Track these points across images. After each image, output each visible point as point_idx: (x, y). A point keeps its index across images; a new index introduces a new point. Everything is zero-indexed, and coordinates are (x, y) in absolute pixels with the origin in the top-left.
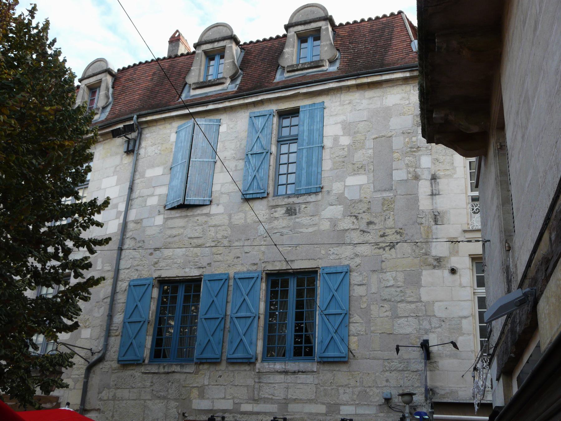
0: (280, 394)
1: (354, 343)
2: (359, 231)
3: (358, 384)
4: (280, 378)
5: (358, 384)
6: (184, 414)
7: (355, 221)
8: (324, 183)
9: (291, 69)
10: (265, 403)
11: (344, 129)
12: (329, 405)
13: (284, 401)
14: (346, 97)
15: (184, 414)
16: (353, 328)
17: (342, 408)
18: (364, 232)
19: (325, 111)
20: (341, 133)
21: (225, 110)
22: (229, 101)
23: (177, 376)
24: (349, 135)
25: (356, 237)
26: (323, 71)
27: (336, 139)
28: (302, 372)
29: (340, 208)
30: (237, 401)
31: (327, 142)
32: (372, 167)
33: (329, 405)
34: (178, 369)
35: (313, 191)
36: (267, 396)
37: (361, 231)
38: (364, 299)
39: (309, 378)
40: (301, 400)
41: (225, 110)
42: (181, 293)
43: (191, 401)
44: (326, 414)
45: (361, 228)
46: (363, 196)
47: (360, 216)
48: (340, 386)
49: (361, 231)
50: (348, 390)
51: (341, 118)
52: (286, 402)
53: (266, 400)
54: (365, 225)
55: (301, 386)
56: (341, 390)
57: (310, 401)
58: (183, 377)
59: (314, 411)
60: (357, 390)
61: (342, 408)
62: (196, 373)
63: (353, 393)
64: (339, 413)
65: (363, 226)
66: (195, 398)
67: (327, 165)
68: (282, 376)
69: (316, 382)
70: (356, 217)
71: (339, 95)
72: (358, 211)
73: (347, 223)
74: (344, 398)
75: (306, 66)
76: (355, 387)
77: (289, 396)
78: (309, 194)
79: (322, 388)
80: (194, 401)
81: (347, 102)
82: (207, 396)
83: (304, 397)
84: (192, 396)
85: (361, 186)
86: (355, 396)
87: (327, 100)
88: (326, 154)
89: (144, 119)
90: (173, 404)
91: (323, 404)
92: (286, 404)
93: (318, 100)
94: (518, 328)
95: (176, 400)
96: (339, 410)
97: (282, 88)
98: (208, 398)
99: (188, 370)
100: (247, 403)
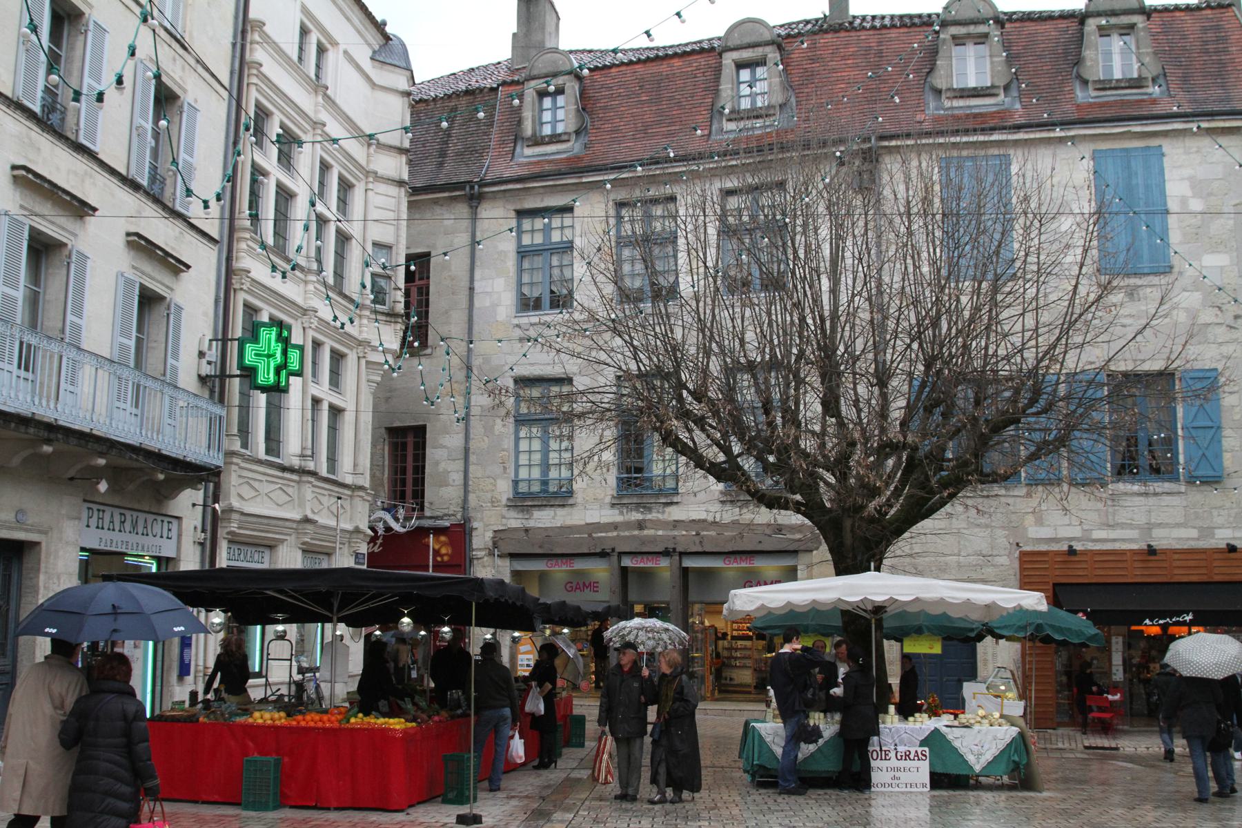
0: (1141, 519)
1: (1228, 460)
2: (1224, 326)
3: (1234, 505)
4: (1137, 500)
5: (1234, 505)
6: (1017, 544)
7: (1219, 313)
8: (1175, 260)
9: (1100, 86)
10: (1122, 528)
11: (1193, 187)
12: (1201, 529)
13: (1146, 526)
14: (1192, 144)
15: (1017, 544)
16: (1226, 443)
17: (1217, 531)
18: (1231, 327)
19: (1165, 159)
20: (1189, 193)
21: (1016, 143)
22: (1026, 132)
23: (1003, 500)
24: (1201, 197)
25: (1221, 333)
26: (1146, 94)
27: (1184, 201)
28: (1168, 493)
29: (1197, 296)
30: (1085, 527)
31: (1173, 205)
32: (1234, 244)
33: (1201, 529)
34: (1003, 492)
35: (1162, 270)
36: (1124, 521)
37: (1228, 326)
38: (1237, 410)
39: (1175, 500)
40: (1167, 524)
41: (1016, 143)
42: (410, 440)
43: (1026, 529)
44: (1198, 539)
45: (1227, 323)
46: (1226, 281)
47: (1224, 308)
48: (1212, 508)
49: (1228, 326)
50: (1222, 512)
51: (1187, 172)
52: (1150, 527)
53: (1122, 526)
54: (1232, 318)
55: (1166, 509)
56: (1215, 513)
57: (1178, 525)
58: (1010, 501)
59: (1183, 536)
60: (1233, 512)
61: (1217, 531)
62: (1029, 495)
63: (1229, 516)
64: (1213, 538)
65: (1230, 321)
66: (1031, 526)
67: (1175, 237)
68: (1141, 498)
69: (1185, 504)
70: (1220, 308)
71: (1181, 138)
72: (1220, 301)
73: (1207, 316)
74: (1219, 520)
75: (1123, 85)
76: (1232, 508)
77: (1153, 521)
78: (1155, 274)
79: (1192, 511)
80: (1030, 529)
81: (1195, 149)
82: (1048, 523)
83: (1170, 521)
84: (1027, 523)
85: (1222, 268)
86: (1231, 519)
87: (1167, 146)
88: (1172, 221)
89: (886, 143)
90: (1000, 533)
91: (1195, 528)
92: (1150, 529)
93: (1154, 142)
94: (1117, 659)
95: (1003, 528)
96: (1214, 534)
97: (1099, 122)
98: (1049, 526)
99: (1016, 494)
100: (1100, 529)
